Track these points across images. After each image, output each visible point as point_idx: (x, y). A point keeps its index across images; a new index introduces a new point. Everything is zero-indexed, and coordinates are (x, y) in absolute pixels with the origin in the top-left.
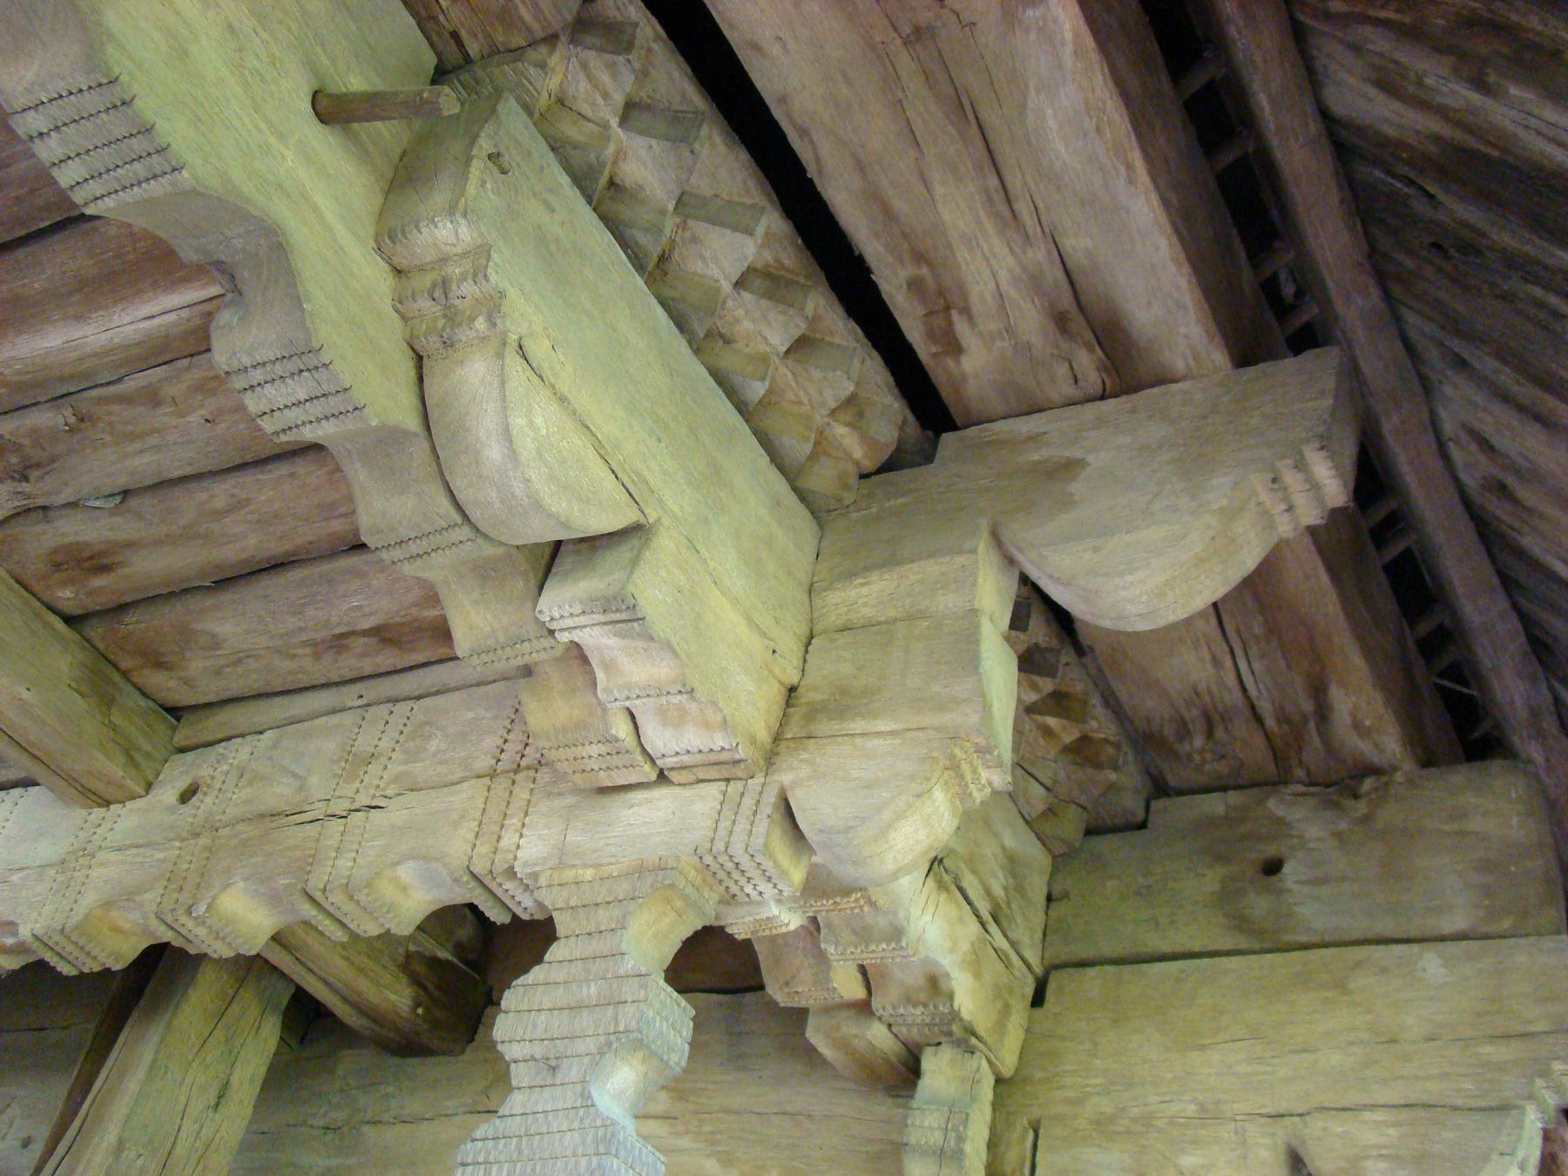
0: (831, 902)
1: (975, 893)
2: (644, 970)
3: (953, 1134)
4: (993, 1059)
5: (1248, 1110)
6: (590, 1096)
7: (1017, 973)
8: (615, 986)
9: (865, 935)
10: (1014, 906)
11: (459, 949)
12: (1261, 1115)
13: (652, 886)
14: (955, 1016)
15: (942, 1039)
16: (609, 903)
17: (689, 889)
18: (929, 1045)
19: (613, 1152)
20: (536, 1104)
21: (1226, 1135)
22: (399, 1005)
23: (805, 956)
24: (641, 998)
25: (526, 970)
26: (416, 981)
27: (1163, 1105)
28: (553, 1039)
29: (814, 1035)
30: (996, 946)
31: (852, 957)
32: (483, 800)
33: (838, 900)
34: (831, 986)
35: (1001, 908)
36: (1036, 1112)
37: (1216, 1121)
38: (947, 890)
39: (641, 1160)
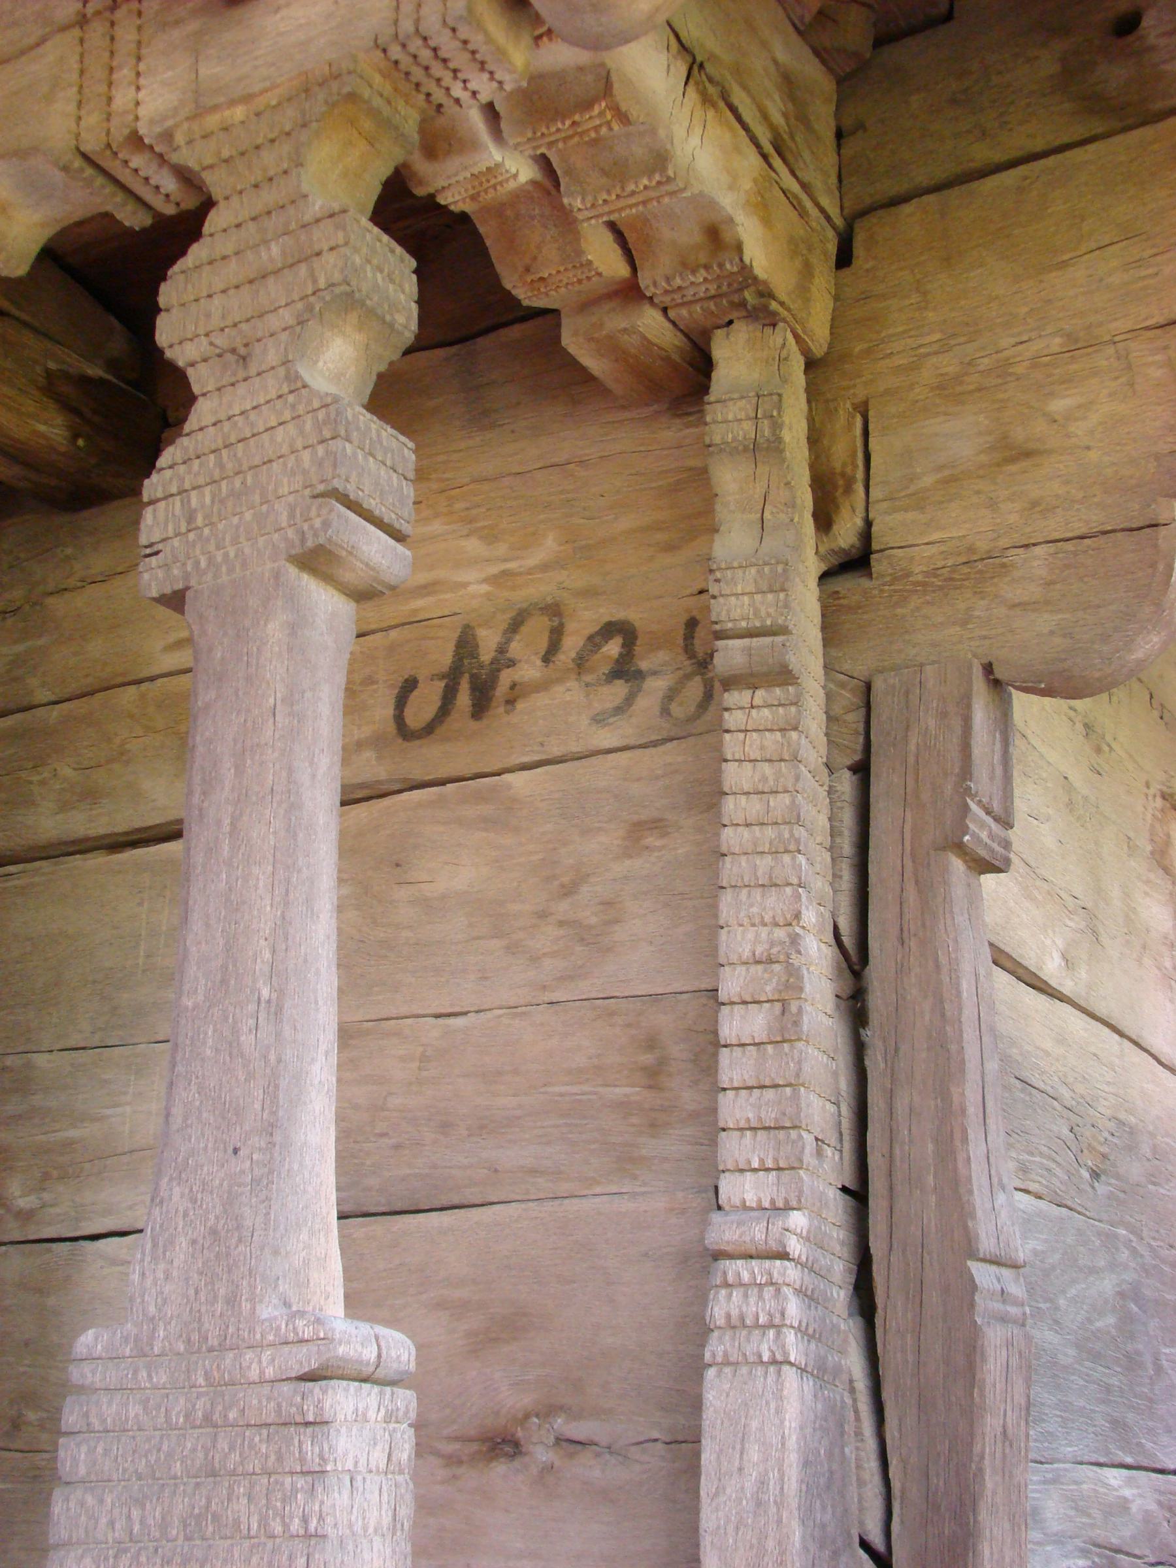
0: (568, 123)
1: (748, 115)
2: (336, 207)
3: (766, 422)
4: (800, 332)
5: (1129, 327)
6: (298, 377)
7: (814, 224)
8: (303, 238)
9: (618, 172)
10: (798, 139)
11: (112, 365)
12: (1147, 328)
13: (326, 102)
14: (745, 270)
15: (734, 315)
16: (273, 141)
17: (377, 102)
18: (719, 327)
19: (343, 433)
20: (230, 406)
21: (1105, 363)
22: (53, 436)
23: (545, 227)
24: (341, 241)
25: (183, 253)
26: (66, 406)
27: (1020, 347)
28: (235, 325)
29: (572, 341)
30: (784, 187)
31: (606, 209)
32: (77, 57)
33: (577, 118)
34: (584, 259)
35: (783, 140)
36: (861, 393)
37: (1090, 350)
38: (714, 105)
39: (381, 443)
